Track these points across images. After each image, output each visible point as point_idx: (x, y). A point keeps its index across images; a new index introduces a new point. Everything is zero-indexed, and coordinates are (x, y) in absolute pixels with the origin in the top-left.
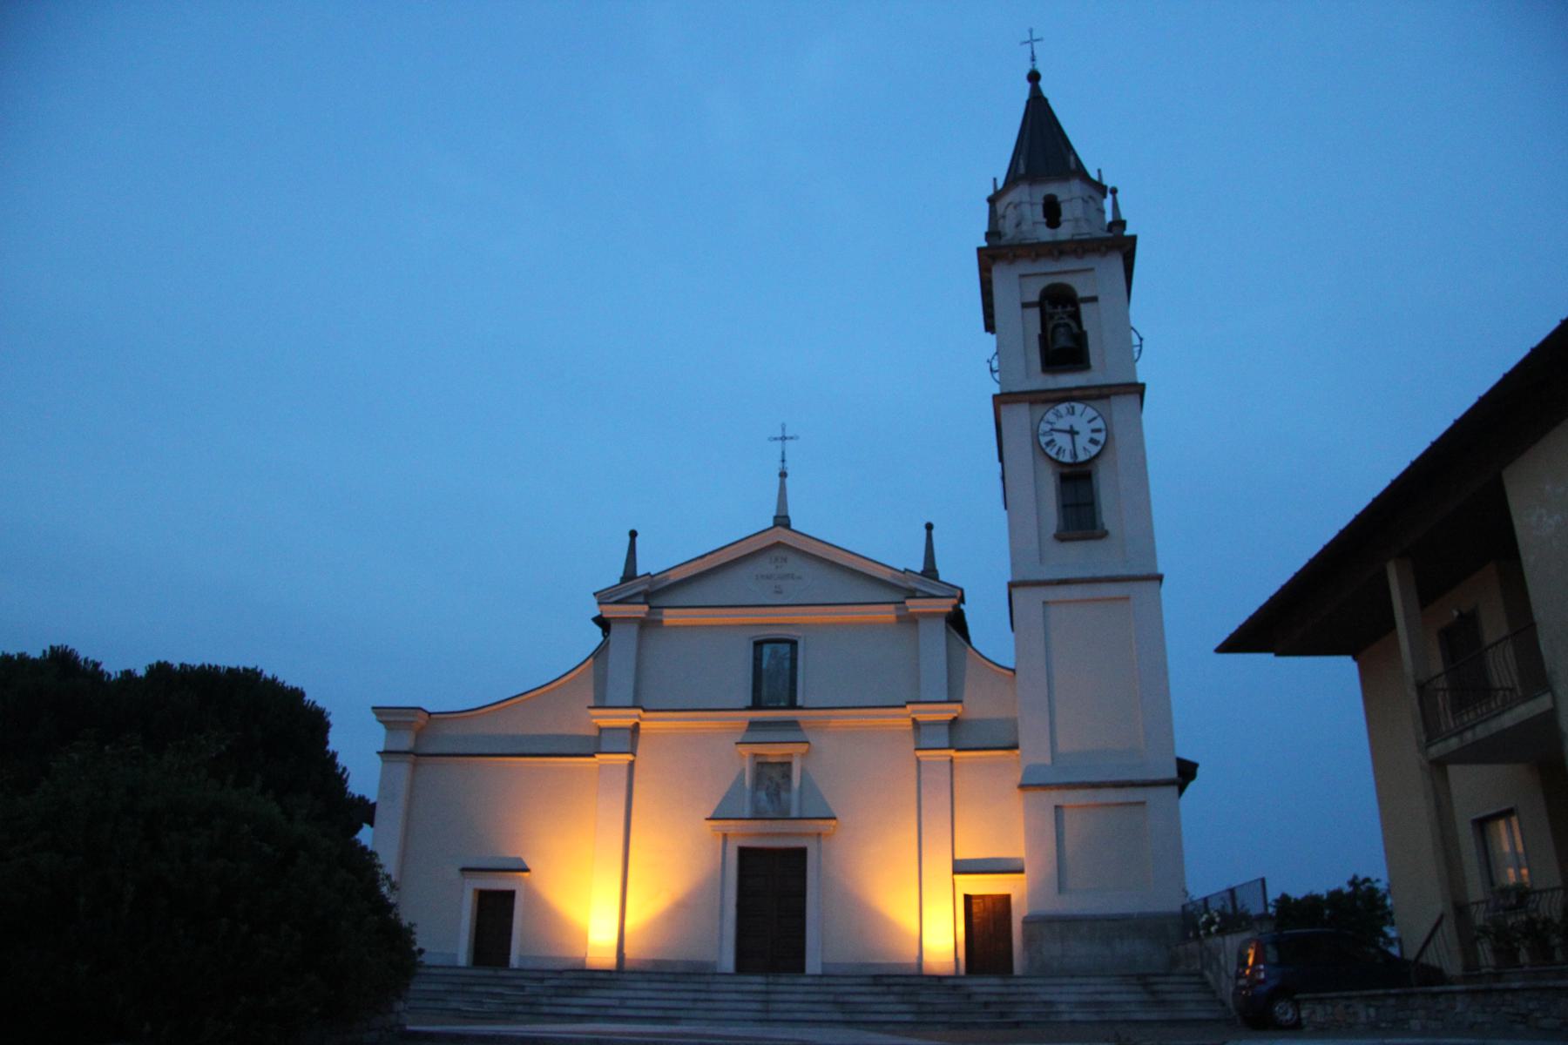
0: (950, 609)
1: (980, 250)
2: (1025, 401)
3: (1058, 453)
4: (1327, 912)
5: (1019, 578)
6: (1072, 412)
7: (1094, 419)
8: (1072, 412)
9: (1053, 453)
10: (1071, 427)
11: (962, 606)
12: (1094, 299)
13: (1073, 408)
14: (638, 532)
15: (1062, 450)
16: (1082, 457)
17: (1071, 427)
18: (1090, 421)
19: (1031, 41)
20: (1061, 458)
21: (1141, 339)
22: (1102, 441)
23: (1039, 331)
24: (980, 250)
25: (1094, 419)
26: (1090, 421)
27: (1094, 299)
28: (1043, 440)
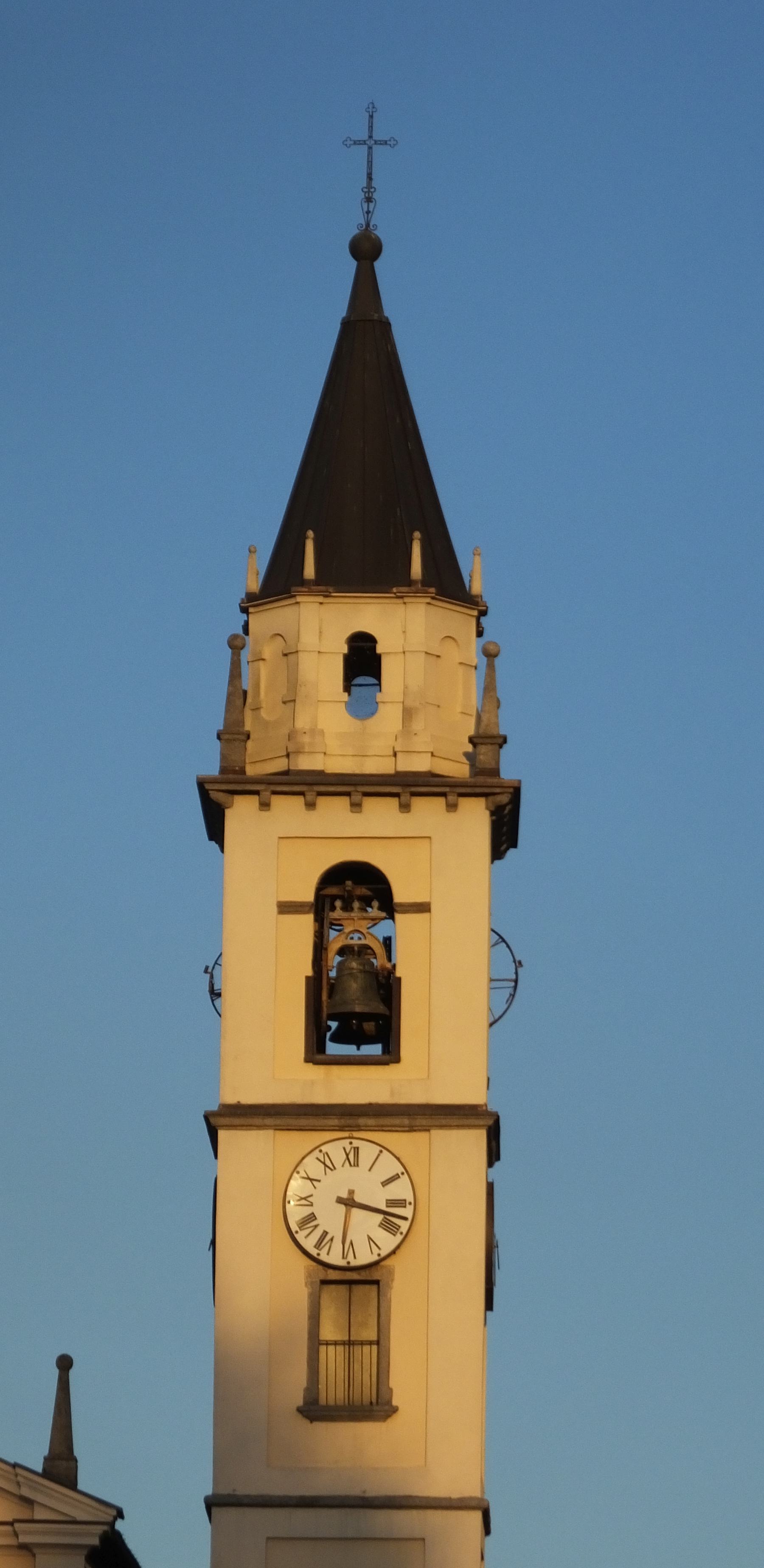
0: (96, 1541)
1: (307, 978)
2: (272, 1129)
3: (318, 1245)
4: (355, 658)
5: (225, 1490)
6: (353, 1159)
7: (396, 1177)
8: (353, 1159)
9: (309, 1244)
10: (351, 1192)
11: (119, 1525)
12: (423, 908)
13: (357, 1150)
14: (64, 1352)
15: (328, 1238)
16: (364, 1257)
17: (351, 1192)
18: (385, 1183)
19: (370, 143)
20: (324, 1257)
21: (519, 964)
22: (410, 1217)
23: (310, 972)
24: (307, 978)
25: (396, 1177)
26: (385, 1183)
27: (423, 908)
28: (296, 1213)
